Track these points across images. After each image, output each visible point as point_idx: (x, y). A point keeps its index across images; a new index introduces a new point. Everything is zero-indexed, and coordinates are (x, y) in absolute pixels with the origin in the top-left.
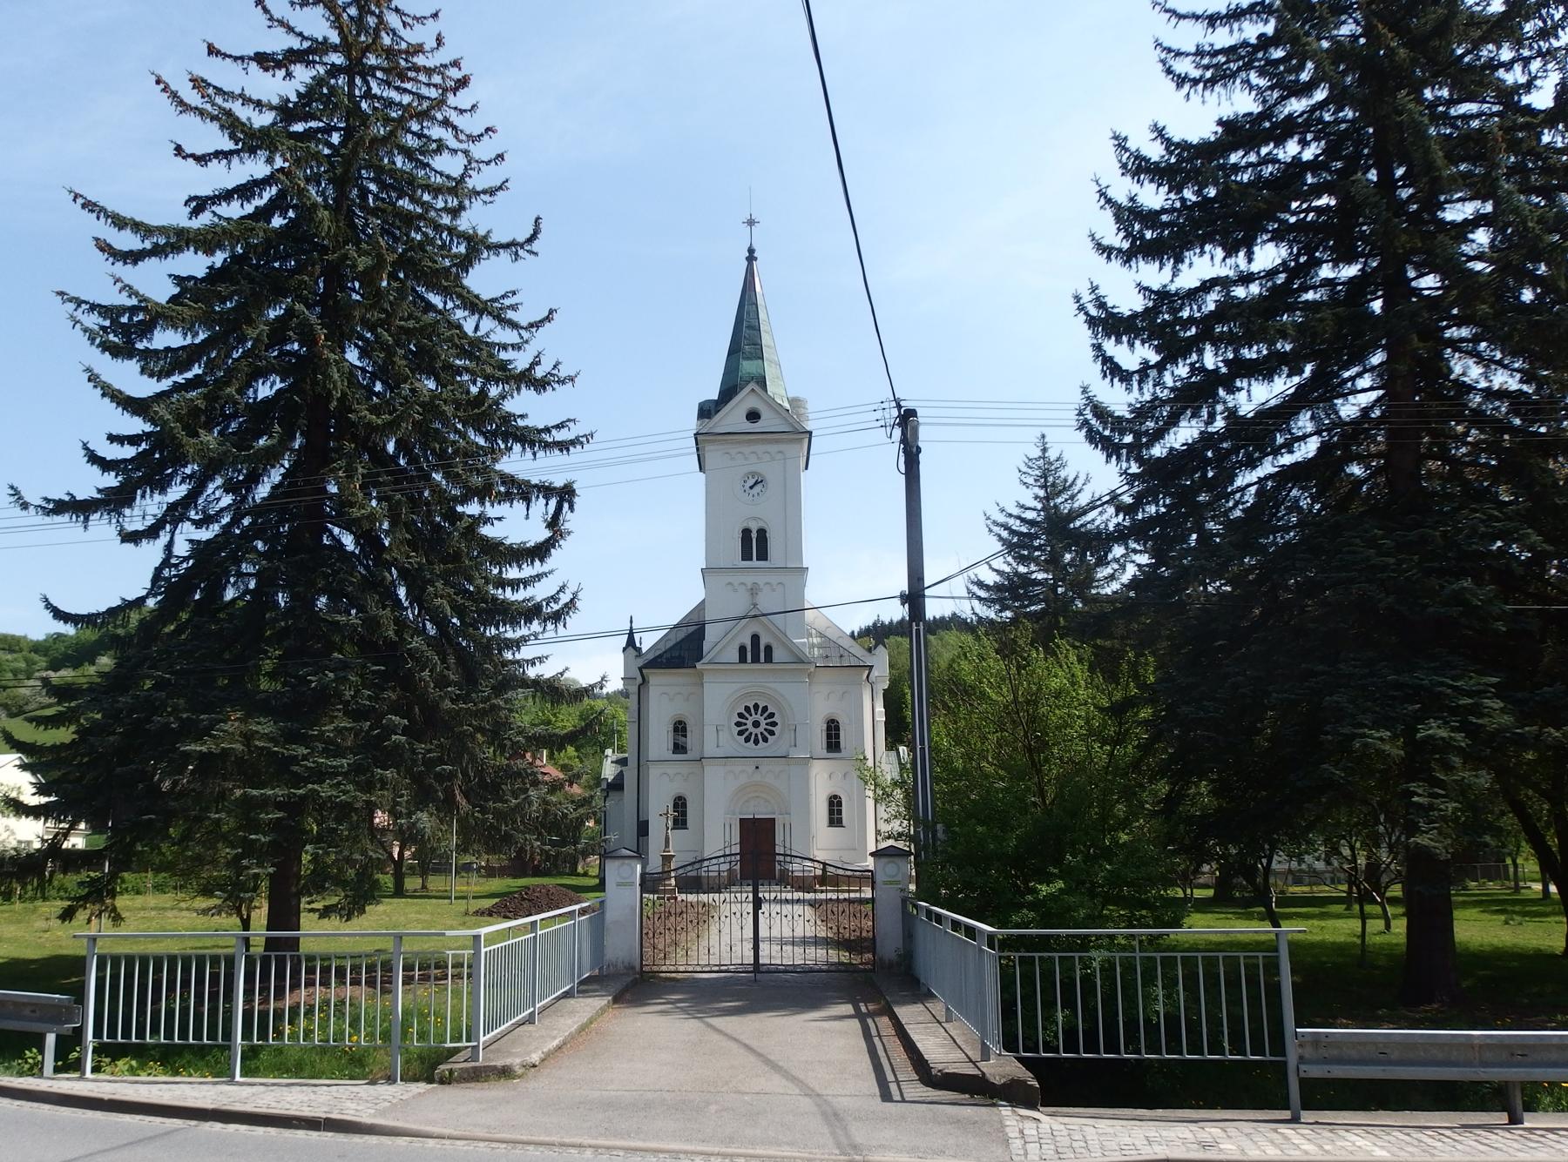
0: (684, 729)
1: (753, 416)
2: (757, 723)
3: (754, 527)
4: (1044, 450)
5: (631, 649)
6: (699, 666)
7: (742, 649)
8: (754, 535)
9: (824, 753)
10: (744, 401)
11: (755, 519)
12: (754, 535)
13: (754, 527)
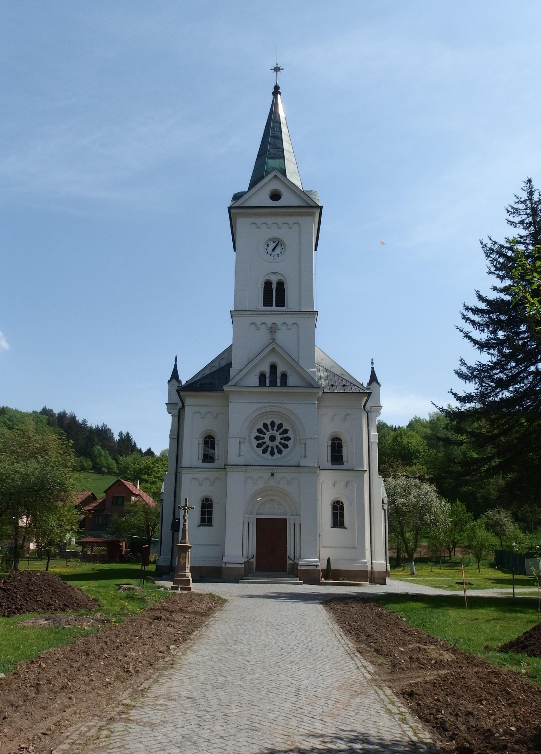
0: (213, 443)
1: (275, 196)
2: (273, 438)
3: (274, 279)
4: (531, 193)
5: (174, 382)
6: (226, 388)
7: (262, 377)
8: (274, 286)
9: (329, 465)
10: (269, 185)
11: (274, 273)
12: (274, 286)
13: (274, 279)
